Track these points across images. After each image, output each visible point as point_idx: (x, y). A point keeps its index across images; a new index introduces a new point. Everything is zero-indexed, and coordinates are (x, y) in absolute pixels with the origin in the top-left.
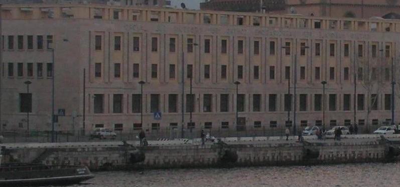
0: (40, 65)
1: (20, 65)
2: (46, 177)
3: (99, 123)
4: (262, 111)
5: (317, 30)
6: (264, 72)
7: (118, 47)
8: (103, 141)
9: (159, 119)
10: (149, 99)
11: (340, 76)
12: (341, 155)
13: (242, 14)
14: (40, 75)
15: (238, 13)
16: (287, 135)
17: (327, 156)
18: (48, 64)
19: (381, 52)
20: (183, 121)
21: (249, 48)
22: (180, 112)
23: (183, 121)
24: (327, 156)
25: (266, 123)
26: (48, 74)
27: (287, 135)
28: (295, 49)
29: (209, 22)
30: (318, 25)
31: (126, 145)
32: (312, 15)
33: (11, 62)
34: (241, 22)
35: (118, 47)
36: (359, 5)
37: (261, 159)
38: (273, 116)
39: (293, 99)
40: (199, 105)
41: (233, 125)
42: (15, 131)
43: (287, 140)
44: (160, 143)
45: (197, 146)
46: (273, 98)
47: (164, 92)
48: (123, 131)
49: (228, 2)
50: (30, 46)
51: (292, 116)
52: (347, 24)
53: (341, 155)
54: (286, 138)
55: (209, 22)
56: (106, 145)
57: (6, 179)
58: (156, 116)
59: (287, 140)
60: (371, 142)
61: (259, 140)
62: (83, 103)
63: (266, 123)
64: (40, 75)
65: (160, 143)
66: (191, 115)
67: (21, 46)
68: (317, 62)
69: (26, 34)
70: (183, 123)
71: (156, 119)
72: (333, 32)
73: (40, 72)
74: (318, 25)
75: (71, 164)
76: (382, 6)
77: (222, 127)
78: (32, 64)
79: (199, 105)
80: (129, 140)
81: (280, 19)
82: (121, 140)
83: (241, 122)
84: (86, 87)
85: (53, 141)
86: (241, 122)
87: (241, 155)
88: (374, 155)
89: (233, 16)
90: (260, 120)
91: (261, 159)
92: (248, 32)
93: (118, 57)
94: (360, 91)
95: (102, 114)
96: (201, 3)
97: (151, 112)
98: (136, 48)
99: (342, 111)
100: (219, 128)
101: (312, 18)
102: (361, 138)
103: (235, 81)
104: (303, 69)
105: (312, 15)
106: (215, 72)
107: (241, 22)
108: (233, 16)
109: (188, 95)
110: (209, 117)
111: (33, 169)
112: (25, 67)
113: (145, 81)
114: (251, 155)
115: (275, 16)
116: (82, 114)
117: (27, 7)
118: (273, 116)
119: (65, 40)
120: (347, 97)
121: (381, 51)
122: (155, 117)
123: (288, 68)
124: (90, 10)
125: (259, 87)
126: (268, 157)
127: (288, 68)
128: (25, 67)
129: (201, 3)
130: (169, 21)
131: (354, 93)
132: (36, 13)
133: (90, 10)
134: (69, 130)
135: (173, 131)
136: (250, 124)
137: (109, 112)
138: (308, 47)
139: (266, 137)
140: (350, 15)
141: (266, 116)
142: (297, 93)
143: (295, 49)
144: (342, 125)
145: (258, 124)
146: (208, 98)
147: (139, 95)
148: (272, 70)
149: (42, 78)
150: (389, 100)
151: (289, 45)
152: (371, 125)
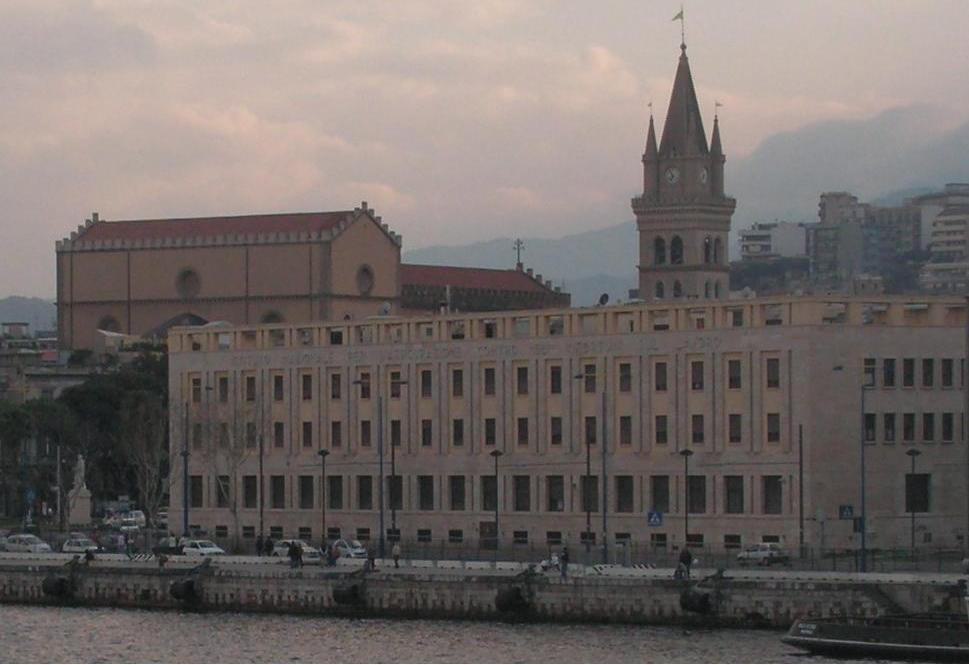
0: (890, 419)
1: (929, 418)
2: (957, 645)
3: (621, 531)
4: (288, 509)
5: (337, 348)
6: (443, 432)
7: (735, 382)
8: (756, 570)
9: (660, 525)
10: (647, 487)
11: (291, 433)
12: (289, 597)
13: (488, 317)
14: (890, 438)
15: (481, 315)
16: (396, 558)
17: (318, 600)
18: (905, 415)
19: (211, 386)
20: (605, 529)
21: (474, 383)
22: (376, 510)
23: (605, 529)
24: (318, 600)
25: (440, 534)
26: (887, 435)
27: (396, 558)
28: (380, 386)
29: (552, 332)
30: (336, 339)
31: (719, 577)
32: (347, 317)
33: (947, 411)
34: (490, 331)
35: (735, 382)
36: (240, 299)
37: (448, 605)
38: (552, 521)
39: (600, 486)
40: (571, 497)
41: (472, 535)
42: (940, 549)
43: (397, 566)
44: (650, 573)
45: (577, 578)
46: (555, 483)
47: (641, 472)
48: (431, 544)
49: (519, 292)
50: (909, 380)
51: (388, 519)
52: (278, 336)
53: (289, 597)
54: (392, 563)
55: (552, 332)
56: (758, 578)
57: (878, 641)
58: (652, 520)
59: (397, 566)
60: (227, 572)
61: (235, 563)
62: (804, 490)
63: (440, 534)
64: (890, 438)
65: (650, 573)
66: (589, 517)
67: (928, 380)
68: (336, 411)
69: (918, 355)
70: (604, 535)
71: (652, 525)
72: (306, 351)
73: (870, 432)
74: (336, 339)
75: (824, 616)
76: (171, 301)
77: (420, 540)
78: (874, 415)
79: (571, 497)
80: (728, 567)
81: (749, 309)
82: (713, 567)
83: (489, 531)
84: (586, 465)
85: (864, 570)
86: (489, 531)
87: (211, 588)
88: (217, 598)
89: (504, 319)
90: (558, 530)
91: (448, 605)
92: (474, 352)
93: (735, 402)
94: (252, 469)
95: (925, 514)
96: (569, 295)
97: (907, 511)
98: (698, 384)
99: (446, 510)
100: (443, 541)
101: (348, 323)
102: (250, 564)
103: (681, 450)
104: (396, 424)
105: (347, 317)
106: (540, 431)
107: (490, 331)
108: (504, 319)
109: (388, 477)
110: (424, 520)
111: (910, 626)
112: (919, 421)
113: (501, 450)
114: (227, 591)
115: (886, 301)
116: (805, 522)
117: (909, 301)
118: (552, 521)
119: (840, 368)
120: (306, 482)
121: (211, 389)
122: (649, 521)
123: (366, 425)
124: (790, 309)
125: (452, 461)
126: (434, 601)
127: (591, 421)
128: (919, 421)
129: (569, 295)
130: (632, 330)
131: (378, 474)
132: (897, 314)
133: (790, 309)
134: (832, 547)
135: (624, 549)
136: (505, 536)
137: (752, 512)
138: (357, 382)
139: (458, 562)
140: (272, 317)
141: (440, 520)
142: (264, 474)
143: (380, 386)
144: (294, 538)
145: (424, 535)
146: (426, 483)
147: (491, 477)
148: (427, 426)
149: (874, 444)
150: (193, 488)
151: (594, 371)
152: (724, 551)
